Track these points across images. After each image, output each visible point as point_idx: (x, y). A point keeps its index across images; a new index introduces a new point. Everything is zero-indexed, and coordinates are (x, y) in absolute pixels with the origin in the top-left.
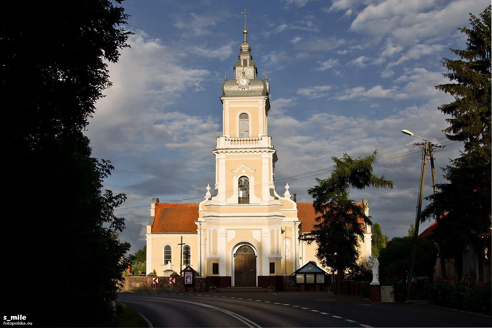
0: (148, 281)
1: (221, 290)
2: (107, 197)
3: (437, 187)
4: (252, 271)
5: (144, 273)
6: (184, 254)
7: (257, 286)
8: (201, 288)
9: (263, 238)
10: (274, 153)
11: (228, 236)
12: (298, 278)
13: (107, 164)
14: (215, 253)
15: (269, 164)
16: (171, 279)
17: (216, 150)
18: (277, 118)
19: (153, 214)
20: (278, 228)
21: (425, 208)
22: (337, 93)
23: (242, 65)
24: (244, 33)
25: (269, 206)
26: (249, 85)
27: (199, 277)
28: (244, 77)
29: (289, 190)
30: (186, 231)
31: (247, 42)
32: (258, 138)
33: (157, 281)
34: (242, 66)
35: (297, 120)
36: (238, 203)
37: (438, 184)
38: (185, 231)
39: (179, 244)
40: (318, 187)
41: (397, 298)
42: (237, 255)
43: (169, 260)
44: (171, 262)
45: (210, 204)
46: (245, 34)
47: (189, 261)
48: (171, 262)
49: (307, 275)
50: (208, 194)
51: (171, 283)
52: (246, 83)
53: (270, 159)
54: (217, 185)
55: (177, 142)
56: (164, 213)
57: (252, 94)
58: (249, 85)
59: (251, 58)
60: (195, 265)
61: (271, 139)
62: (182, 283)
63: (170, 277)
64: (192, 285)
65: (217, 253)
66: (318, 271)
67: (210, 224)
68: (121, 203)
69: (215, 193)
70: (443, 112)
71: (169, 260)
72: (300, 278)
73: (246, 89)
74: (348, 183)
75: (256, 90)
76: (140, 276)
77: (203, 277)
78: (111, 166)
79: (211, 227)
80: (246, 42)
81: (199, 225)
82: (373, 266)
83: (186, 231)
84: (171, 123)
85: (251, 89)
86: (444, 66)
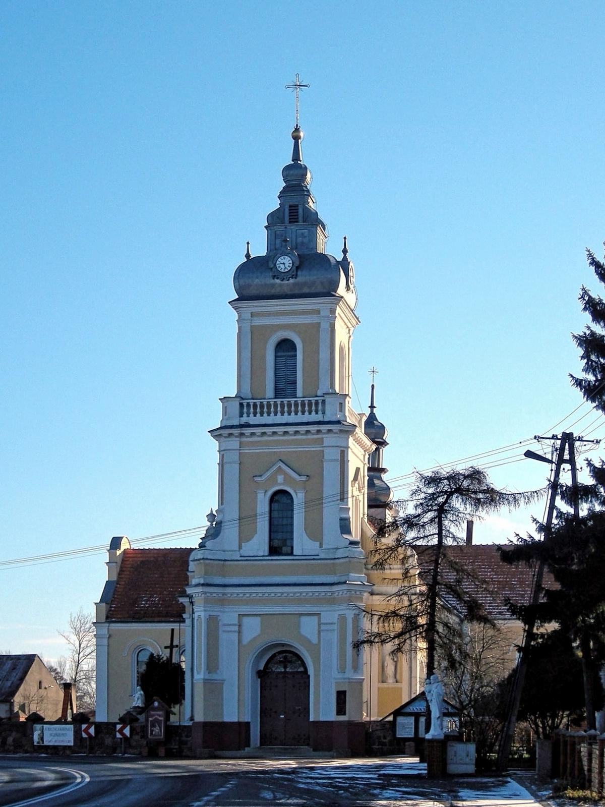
11: (245, 629)
16: (119, 727)
33: (92, 731)
36: (267, 553)
51: (118, 736)
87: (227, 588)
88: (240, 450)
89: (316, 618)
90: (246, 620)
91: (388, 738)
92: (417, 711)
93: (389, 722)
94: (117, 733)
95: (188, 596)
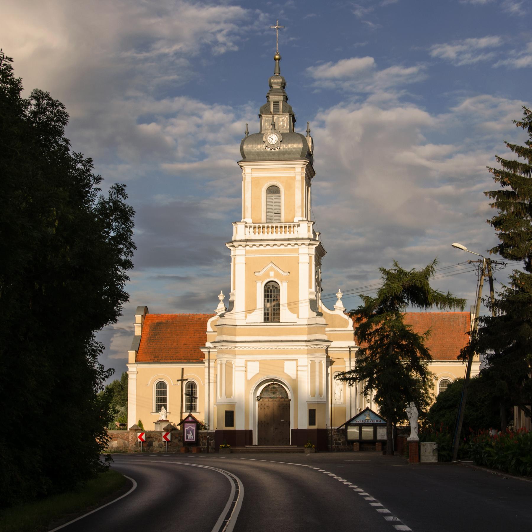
0: (130, 438)
1: (236, 450)
2: (99, 369)
3: (479, 321)
4: (283, 421)
5: (124, 425)
6: (186, 394)
7: (291, 444)
8: (208, 448)
9: (299, 373)
10: (317, 246)
12: (364, 431)
13: (99, 345)
14: (229, 395)
15: (310, 263)
16: (164, 434)
17: (232, 242)
18: (384, 109)
19: (138, 332)
20: (321, 359)
21: (467, 345)
22: (513, 52)
23: (272, 110)
24: (275, 59)
25: (309, 326)
26: (281, 144)
27: (206, 431)
28: (273, 131)
29: (341, 299)
30: (190, 359)
31: (279, 74)
32: (294, 223)
33: (144, 437)
34: (271, 113)
35: (425, 111)
36: (263, 321)
37: (481, 317)
38: (188, 359)
39: (178, 381)
40: (363, 307)
41: (440, 458)
42: (261, 398)
43: (163, 405)
44: (166, 408)
45: (222, 324)
46: (277, 61)
47: (195, 405)
48: (166, 408)
49: (363, 427)
50: (221, 307)
51: (164, 440)
52: (277, 140)
53: (311, 255)
54: (233, 295)
55: (183, 160)
56: (156, 331)
57: (286, 156)
58: (281, 144)
59: (286, 99)
60: (200, 416)
61: (313, 225)
62: (179, 441)
63: (163, 432)
64: (196, 443)
65: (232, 395)
66: (379, 422)
67: (221, 352)
68: (111, 375)
69: (230, 306)
70: (493, 226)
71: (163, 405)
72: (367, 431)
73: (277, 150)
74: (406, 301)
75: (292, 151)
76: (117, 430)
77: (211, 431)
78: (103, 346)
79: (223, 358)
80: (278, 74)
81: (206, 354)
82: (411, 417)
83: (190, 359)
84: (173, 120)
85: (284, 148)
86: (491, 172)
87: (237, 343)
88: (245, 255)
89: (295, 362)
90: (249, 363)
91: (342, 440)
92: (360, 422)
93: (342, 429)
94: (163, 438)
95: (207, 348)
